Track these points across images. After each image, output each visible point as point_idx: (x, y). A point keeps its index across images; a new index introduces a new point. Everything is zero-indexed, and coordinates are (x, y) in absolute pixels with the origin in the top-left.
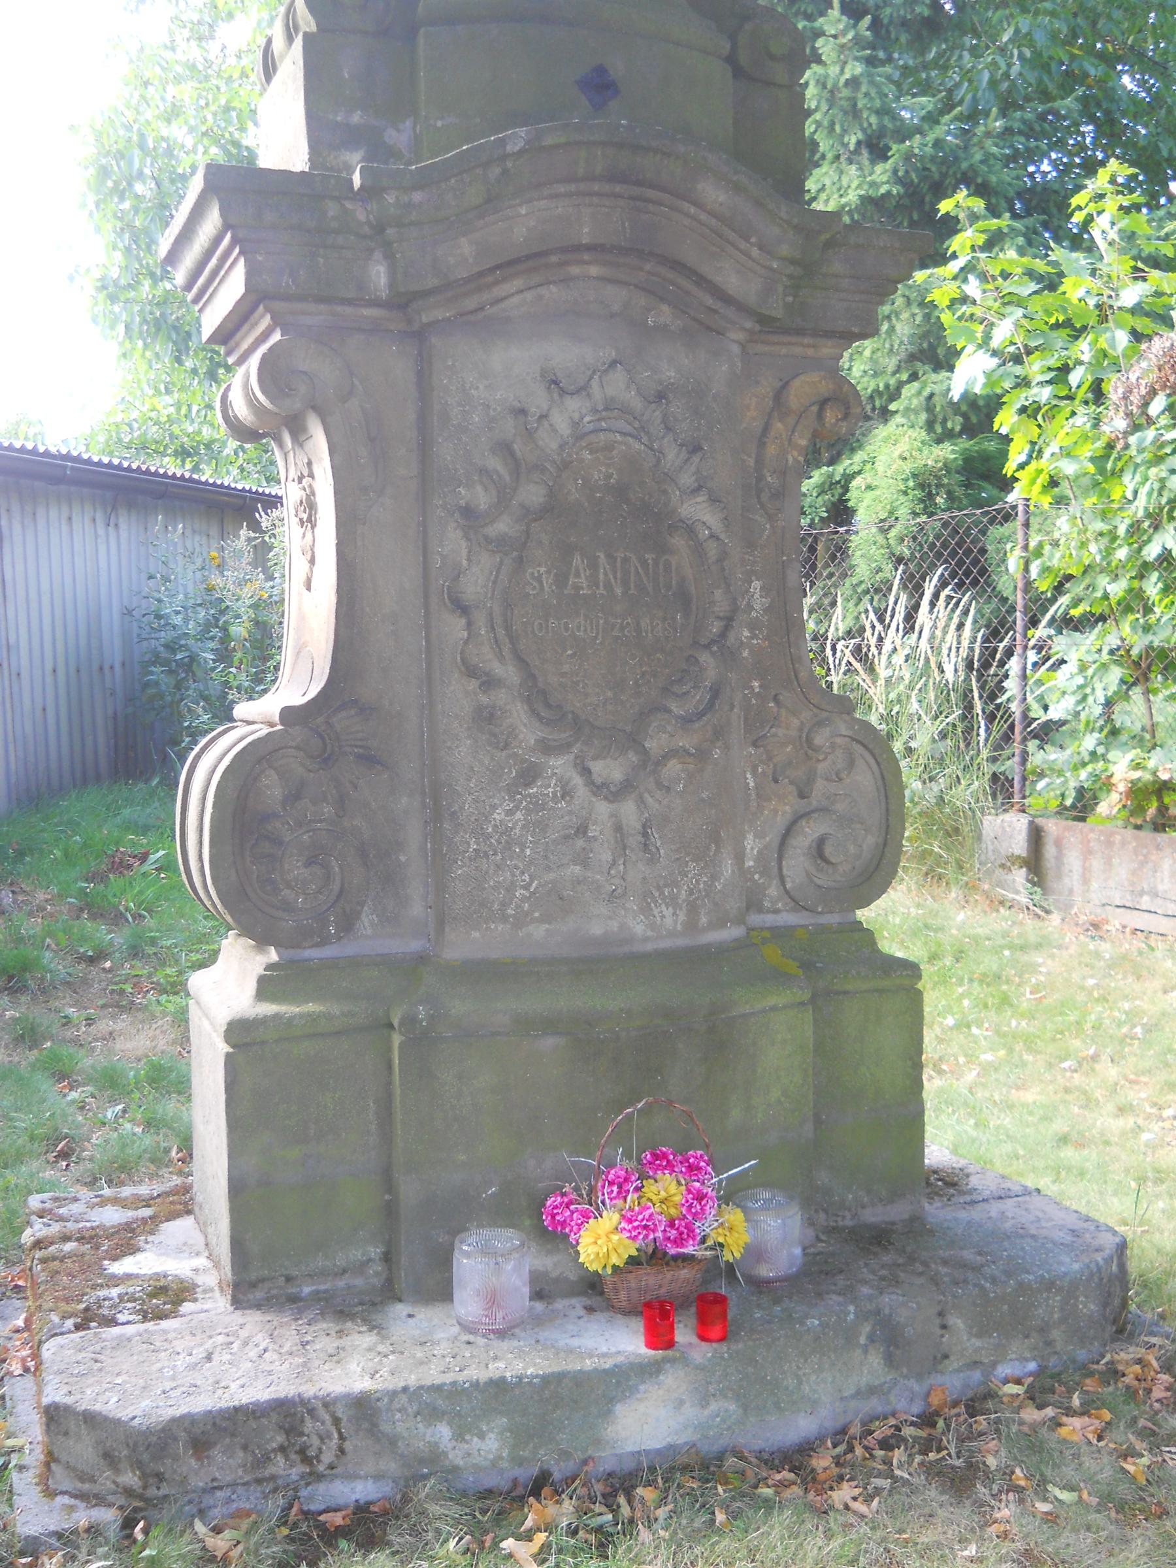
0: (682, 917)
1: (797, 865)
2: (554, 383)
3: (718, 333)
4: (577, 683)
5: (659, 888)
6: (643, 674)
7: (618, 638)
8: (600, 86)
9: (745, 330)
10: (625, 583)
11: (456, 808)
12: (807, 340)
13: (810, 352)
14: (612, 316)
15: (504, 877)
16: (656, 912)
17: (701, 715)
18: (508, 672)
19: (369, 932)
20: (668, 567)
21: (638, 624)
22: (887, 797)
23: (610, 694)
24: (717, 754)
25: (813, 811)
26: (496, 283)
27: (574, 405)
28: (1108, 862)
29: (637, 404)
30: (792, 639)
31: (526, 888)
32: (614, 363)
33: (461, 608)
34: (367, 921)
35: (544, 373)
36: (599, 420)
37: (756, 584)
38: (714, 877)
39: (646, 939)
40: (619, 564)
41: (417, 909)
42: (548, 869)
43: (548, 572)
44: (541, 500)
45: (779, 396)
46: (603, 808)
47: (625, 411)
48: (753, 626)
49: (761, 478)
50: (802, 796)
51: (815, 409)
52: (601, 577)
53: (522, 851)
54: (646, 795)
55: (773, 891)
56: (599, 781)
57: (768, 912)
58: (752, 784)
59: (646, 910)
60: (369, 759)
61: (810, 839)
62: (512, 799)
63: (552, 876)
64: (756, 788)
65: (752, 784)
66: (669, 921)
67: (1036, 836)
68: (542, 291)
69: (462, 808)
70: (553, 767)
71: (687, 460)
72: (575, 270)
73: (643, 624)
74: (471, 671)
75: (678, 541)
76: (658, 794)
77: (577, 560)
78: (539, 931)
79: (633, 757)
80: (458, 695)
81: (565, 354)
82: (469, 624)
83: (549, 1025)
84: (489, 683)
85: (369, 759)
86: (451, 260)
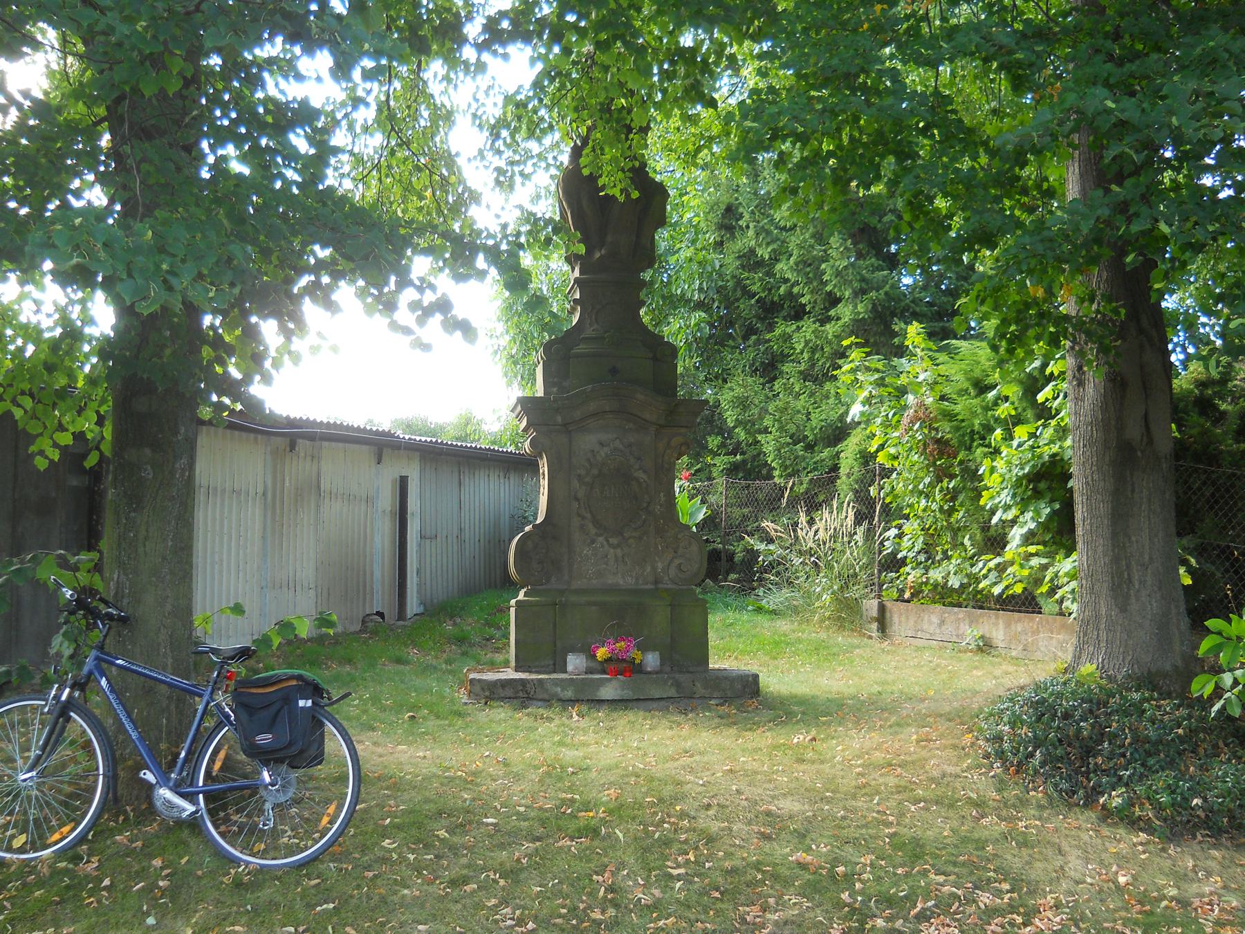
2: (601, 444)
8: (614, 371)
18: (588, 515)
27: (606, 449)
28: (907, 618)
33: (577, 500)
34: (553, 579)
41: (566, 577)
67: (882, 608)
74: (579, 515)
78: (594, 582)
80: (576, 521)
81: (604, 437)
83: (595, 604)
84: (583, 518)
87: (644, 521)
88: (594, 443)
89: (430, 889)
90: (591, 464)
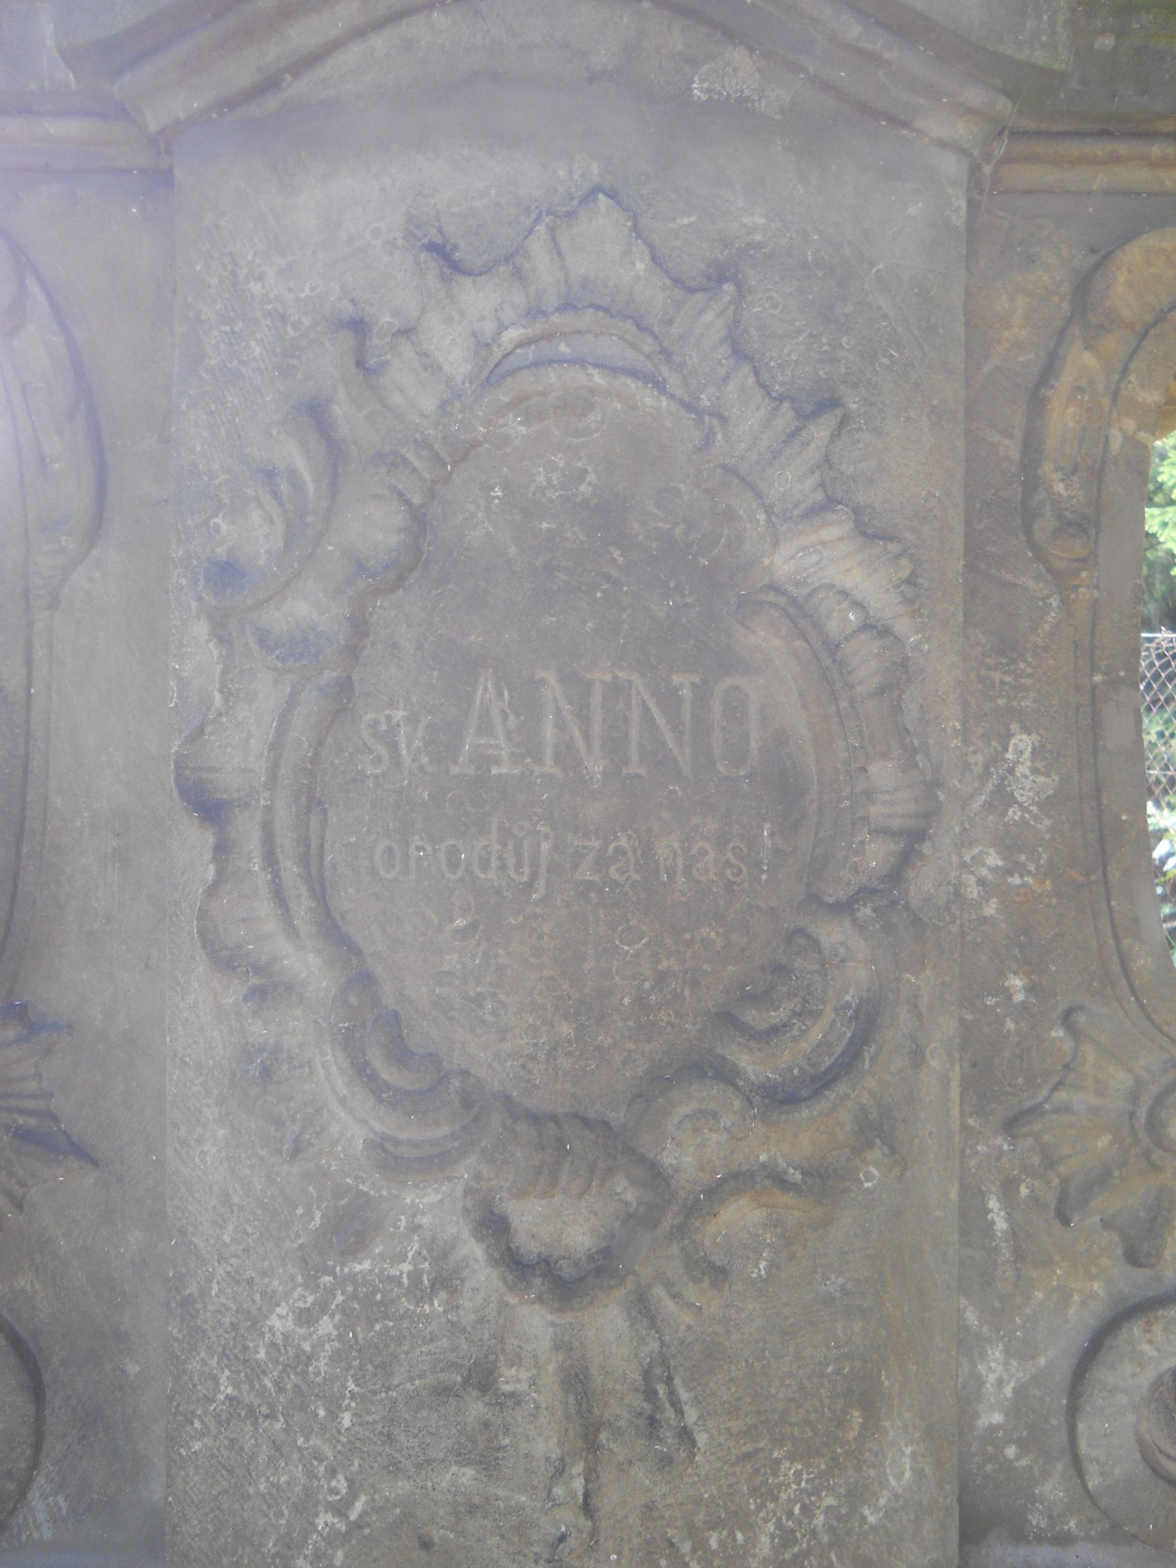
3: (896, 121)
5: (691, 1530)
6: (662, 978)
7: (589, 885)
9: (971, 111)
11: (193, 1289)
18: (306, 964)
19: (47, 1534)
23: (566, 1029)
24: (872, 1174)
27: (481, 300)
30: (1115, 876)
31: (340, 1509)
32: (595, 190)
33: (209, 808)
36: (549, 336)
37: (1022, 743)
38: (857, 1496)
40: (596, 699)
42: (394, 1469)
43: (412, 720)
44: (394, 540)
45: (1084, 289)
46: (537, 1323)
49: (1030, 479)
50: (1133, 1257)
52: (549, 733)
53: (333, 1415)
54: (659, 1291)
55: (1053, 1489)
57: (1040, 1539)
58: (1001, 1225)
61: (1151, 1374)
62: (311, 1283)
63: (403, 1487)
64: (1014, 1233)
65: (1001, 1225)
68: (411, 28)
69: (204, 1292)
74: (226, 960)
75: (764, 639)
76: (691, 1292)
77: (485, 689)
81: (466, 182)
82: (221, 849)
84: (269, 990)
87: (866, 1022)
89: (495, 1549)
90: (334, 454)
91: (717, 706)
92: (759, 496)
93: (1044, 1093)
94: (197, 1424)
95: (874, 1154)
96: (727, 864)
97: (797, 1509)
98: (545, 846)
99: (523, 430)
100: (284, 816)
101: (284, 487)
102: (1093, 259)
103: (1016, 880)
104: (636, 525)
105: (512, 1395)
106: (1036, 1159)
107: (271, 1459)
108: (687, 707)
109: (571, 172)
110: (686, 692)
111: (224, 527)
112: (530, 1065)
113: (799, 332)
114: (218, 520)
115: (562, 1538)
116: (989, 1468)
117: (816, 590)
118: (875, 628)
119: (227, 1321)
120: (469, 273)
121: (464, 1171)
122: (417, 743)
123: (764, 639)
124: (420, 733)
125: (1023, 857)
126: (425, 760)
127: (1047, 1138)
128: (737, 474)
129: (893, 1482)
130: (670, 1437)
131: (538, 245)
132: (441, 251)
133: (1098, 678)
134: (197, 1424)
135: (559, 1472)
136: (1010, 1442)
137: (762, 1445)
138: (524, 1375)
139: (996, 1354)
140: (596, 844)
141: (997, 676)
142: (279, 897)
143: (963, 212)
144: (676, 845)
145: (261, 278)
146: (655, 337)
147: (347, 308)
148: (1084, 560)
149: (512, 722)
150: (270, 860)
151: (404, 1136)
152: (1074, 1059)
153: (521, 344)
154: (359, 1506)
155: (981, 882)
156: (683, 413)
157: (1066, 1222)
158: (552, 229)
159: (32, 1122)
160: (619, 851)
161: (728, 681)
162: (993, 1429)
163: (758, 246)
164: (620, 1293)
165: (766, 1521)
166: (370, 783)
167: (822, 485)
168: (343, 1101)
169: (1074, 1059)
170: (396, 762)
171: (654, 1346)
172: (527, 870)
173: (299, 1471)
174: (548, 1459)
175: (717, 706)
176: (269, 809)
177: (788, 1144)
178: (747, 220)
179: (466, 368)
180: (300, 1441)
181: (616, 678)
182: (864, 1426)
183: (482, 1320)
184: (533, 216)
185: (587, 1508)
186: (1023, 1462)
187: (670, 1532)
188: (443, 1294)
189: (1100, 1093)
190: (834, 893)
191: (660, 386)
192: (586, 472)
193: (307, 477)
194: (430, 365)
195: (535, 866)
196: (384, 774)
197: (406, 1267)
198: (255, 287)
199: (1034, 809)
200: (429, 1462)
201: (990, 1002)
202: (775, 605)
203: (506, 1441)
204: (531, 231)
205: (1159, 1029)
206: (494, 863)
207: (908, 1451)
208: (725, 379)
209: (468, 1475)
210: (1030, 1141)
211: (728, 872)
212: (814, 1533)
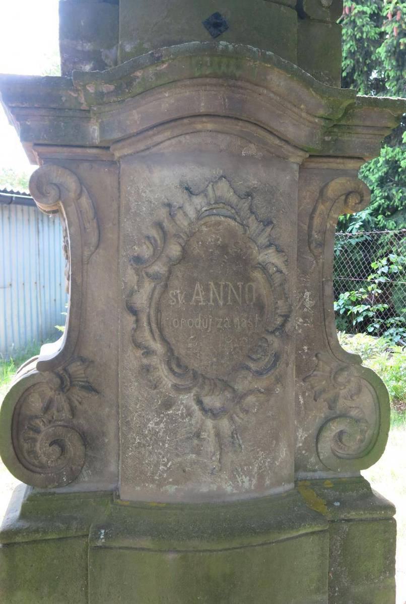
0: (254, 482)
1: (327, 445)
2: (189, 191)
4: (196, 354)
7: (220, 329)
10: (225, 298)
12: (339, 160)
13: (341, 167)
14: (221, 151)
15: (154, 458)
16: (239, 480)
17: (269, 370)
18: (158, 346)
20: (250, 289)
21: (232, 321)
22: (380, 409)
23: (215, 360)
24: (278, 390)
25: (336, 417)
26: (154, 135)
27: (198, 201)
29: (234, 199)
30: (327, 323)
31: (165, 465)
32: (222, 177)
35: (181, 183)
37: (307, 294)
38: (274, 459)
39: (232, 494)
42: (177, 455)
43: (181, 293)
44: (178, 253)
45: (322, 192)
46: (209, 423)
47: (228, 204)
48: (305, 317)
49: (310, 236)
50: (330, 408)
51: (343, 197)
52: (211, 295)
53: (163, 445)
54: (235, 415)
55: (313, 460)
56: (207, 407)
57: (310, 471)
58: (302, 402)
59: (233, 478)
60: (90, 388)
61: (333, 434)
62: (158, 416)
63: (179, 459)
64: (304, 403)
65: (302, 402)
66: (246, 484)
68: (182, 138)
69: (132, 419)
70: (182, 400)
71: (263, 230)
72: (199, 126)
73: (235, 321)
74: (138, 346)
75: (258, 275)
76: (241, 415)
77: (198, 286)
78: (171, 489)
79: (228, 395)
81: (193, 173)
82: (137, 321)
84: (148, 352)
85: (90, 388)
86: (128, 122)
88: (165, 181)
91: (247, 289)
92: (256, 244)
93: (311, 372)
94: (130, 449)
95: (279, 386)
96: (249, 323)
97: (262, 461)
98: (211, 320)
99: (205, 229)
100: (152, 313)
101: (153, 241)
102: (324, 184)
103: (306, 325)
104: (230, 250)
105: (203, 438)
106: (310, 387)
107: (149, 455)
108: (240, 289)
109: (216, 172)
110: (240, 286)
111: (136, 249)
112: (207, 368)
113: (264, 206)
114: (135, 247)
115: (214, 468)
116: (299, 456)
117: (268, 263)
118: (279, 271)
119: (138, 426)
120: (194, 195)
121: (194, 392)
122: (182, 298)
123: (258, 275)
124: (183, 295)
125: (307, 320)
126: (184, 301)
127: (312, 382)
128: (251, 239)
129: (281, 456)
130: (237, 445)
131: (210, 189)
132: (187, 189)
133: (324, 279)
134: (130, 449)
135: (214, 454)
136: (303, 450)
137: (255, 448)
138: (206, 434)
139: (301, 430)
140: (221, 320)
141: (302, 279)
142: (151, 331)
143: (298, 177)
144: (238, 320)
145: (145, 192)
146: (234, 209)
147: (166, 201)
148: (321, 253)
149: (203, 293)
150: (149, 324)
151: (180, 383)
152: (318, 364)
153: (206, 210)
154: (170, 464)
155: (298, 325)
156: (240, 226)
157: (316, 401)
158: (213, 185)
159: (83, 384)
160: (226, 321)
161: (249, 284)
162: (300, 447)
163: (256, 188)
164: (227, 416)
165: (256, 464)
166: (172, 306)
167: (269, 240)
168: (166, 377)
169: (318, 364)
170: (178, 302)
171: (234, 427)
172: (207, 325)
173: (155, 457)
174: (211, 452)
175: (247, 289)
176: (149, 312)
177: (261, 384)
178: (253, 182)
179: (194, 216)
180: (156, 451)
181: (226, 283)
182: (276, 444)
183: (197, 423)
184: (208, 182)
185: (220, 462)
186: (306, 454)
187: (237, 467)
188: (189, 417)
189: (323, 371)
190: (270, 329)
191: (235, 220)
192: (219, 239)
193: (158, 239)
194: (185, 214)
195: (208, 324)
196: (175, 305)
197: (180, 412)
198: (143, 194)
199: (310, 309)
200: (185, 453)
201: (300, 352)
202: (259, 267)
203: (202, 448)
204: (208, 186)
205: (336, 357)
206: (200, 324)
207: (285, 449)
208: (249, 218)
209: (194, 456)
210: (308, 383)
211: (249, 325)
212: (265, 467)
